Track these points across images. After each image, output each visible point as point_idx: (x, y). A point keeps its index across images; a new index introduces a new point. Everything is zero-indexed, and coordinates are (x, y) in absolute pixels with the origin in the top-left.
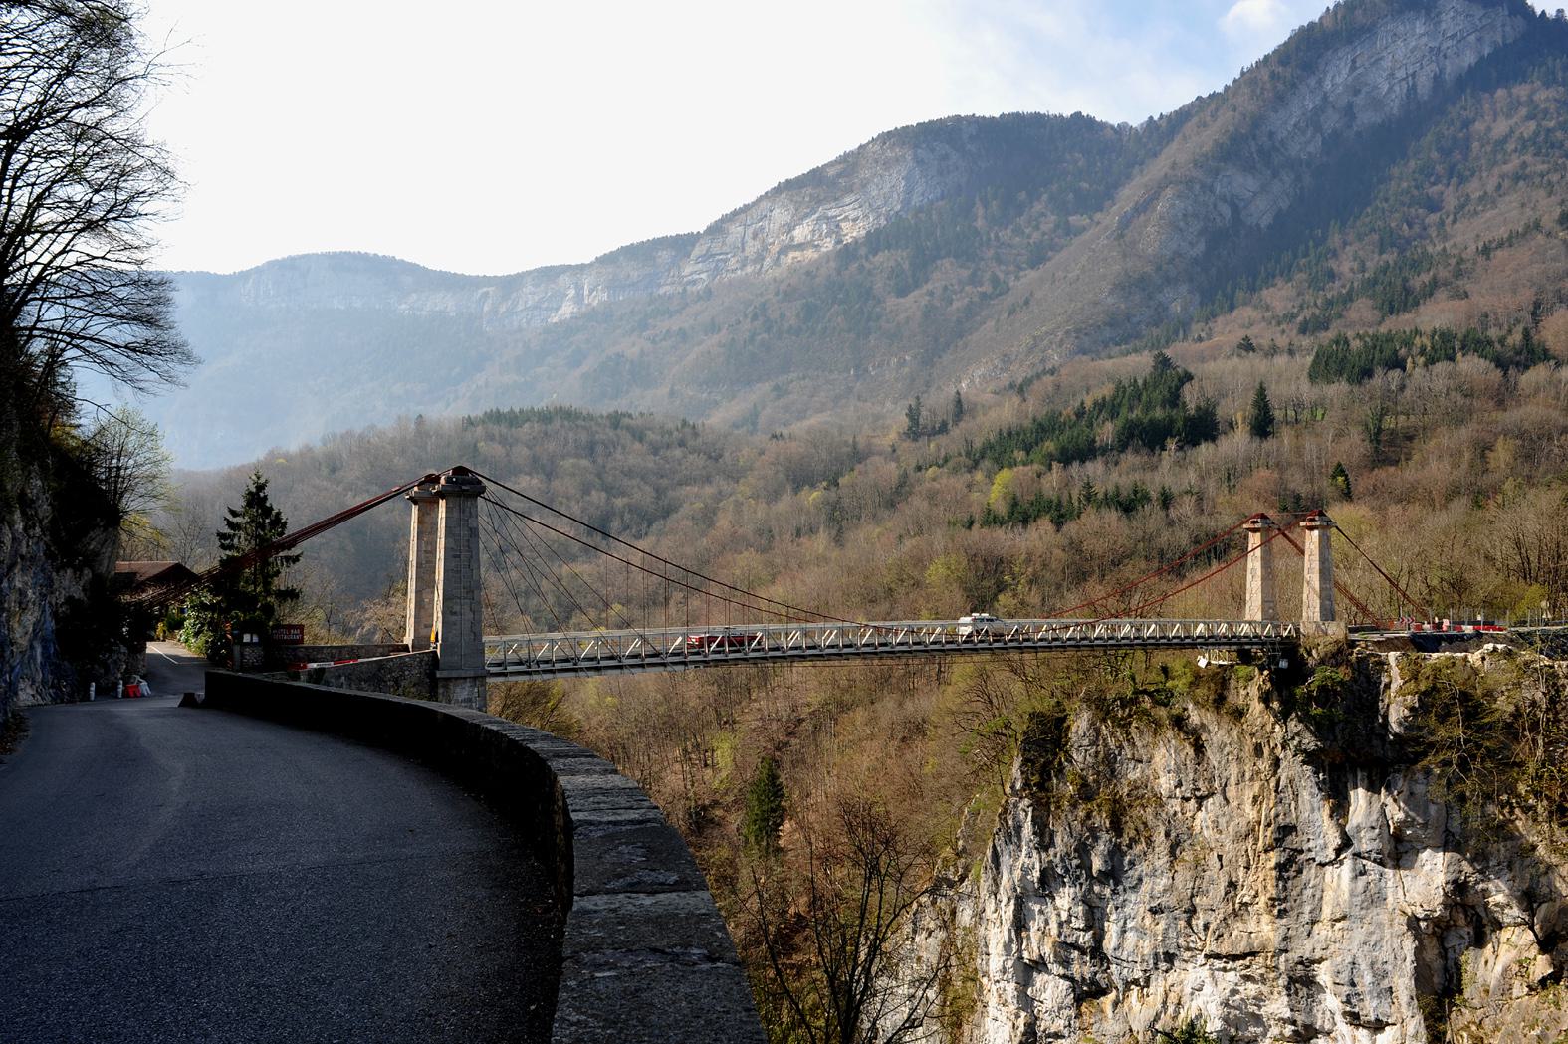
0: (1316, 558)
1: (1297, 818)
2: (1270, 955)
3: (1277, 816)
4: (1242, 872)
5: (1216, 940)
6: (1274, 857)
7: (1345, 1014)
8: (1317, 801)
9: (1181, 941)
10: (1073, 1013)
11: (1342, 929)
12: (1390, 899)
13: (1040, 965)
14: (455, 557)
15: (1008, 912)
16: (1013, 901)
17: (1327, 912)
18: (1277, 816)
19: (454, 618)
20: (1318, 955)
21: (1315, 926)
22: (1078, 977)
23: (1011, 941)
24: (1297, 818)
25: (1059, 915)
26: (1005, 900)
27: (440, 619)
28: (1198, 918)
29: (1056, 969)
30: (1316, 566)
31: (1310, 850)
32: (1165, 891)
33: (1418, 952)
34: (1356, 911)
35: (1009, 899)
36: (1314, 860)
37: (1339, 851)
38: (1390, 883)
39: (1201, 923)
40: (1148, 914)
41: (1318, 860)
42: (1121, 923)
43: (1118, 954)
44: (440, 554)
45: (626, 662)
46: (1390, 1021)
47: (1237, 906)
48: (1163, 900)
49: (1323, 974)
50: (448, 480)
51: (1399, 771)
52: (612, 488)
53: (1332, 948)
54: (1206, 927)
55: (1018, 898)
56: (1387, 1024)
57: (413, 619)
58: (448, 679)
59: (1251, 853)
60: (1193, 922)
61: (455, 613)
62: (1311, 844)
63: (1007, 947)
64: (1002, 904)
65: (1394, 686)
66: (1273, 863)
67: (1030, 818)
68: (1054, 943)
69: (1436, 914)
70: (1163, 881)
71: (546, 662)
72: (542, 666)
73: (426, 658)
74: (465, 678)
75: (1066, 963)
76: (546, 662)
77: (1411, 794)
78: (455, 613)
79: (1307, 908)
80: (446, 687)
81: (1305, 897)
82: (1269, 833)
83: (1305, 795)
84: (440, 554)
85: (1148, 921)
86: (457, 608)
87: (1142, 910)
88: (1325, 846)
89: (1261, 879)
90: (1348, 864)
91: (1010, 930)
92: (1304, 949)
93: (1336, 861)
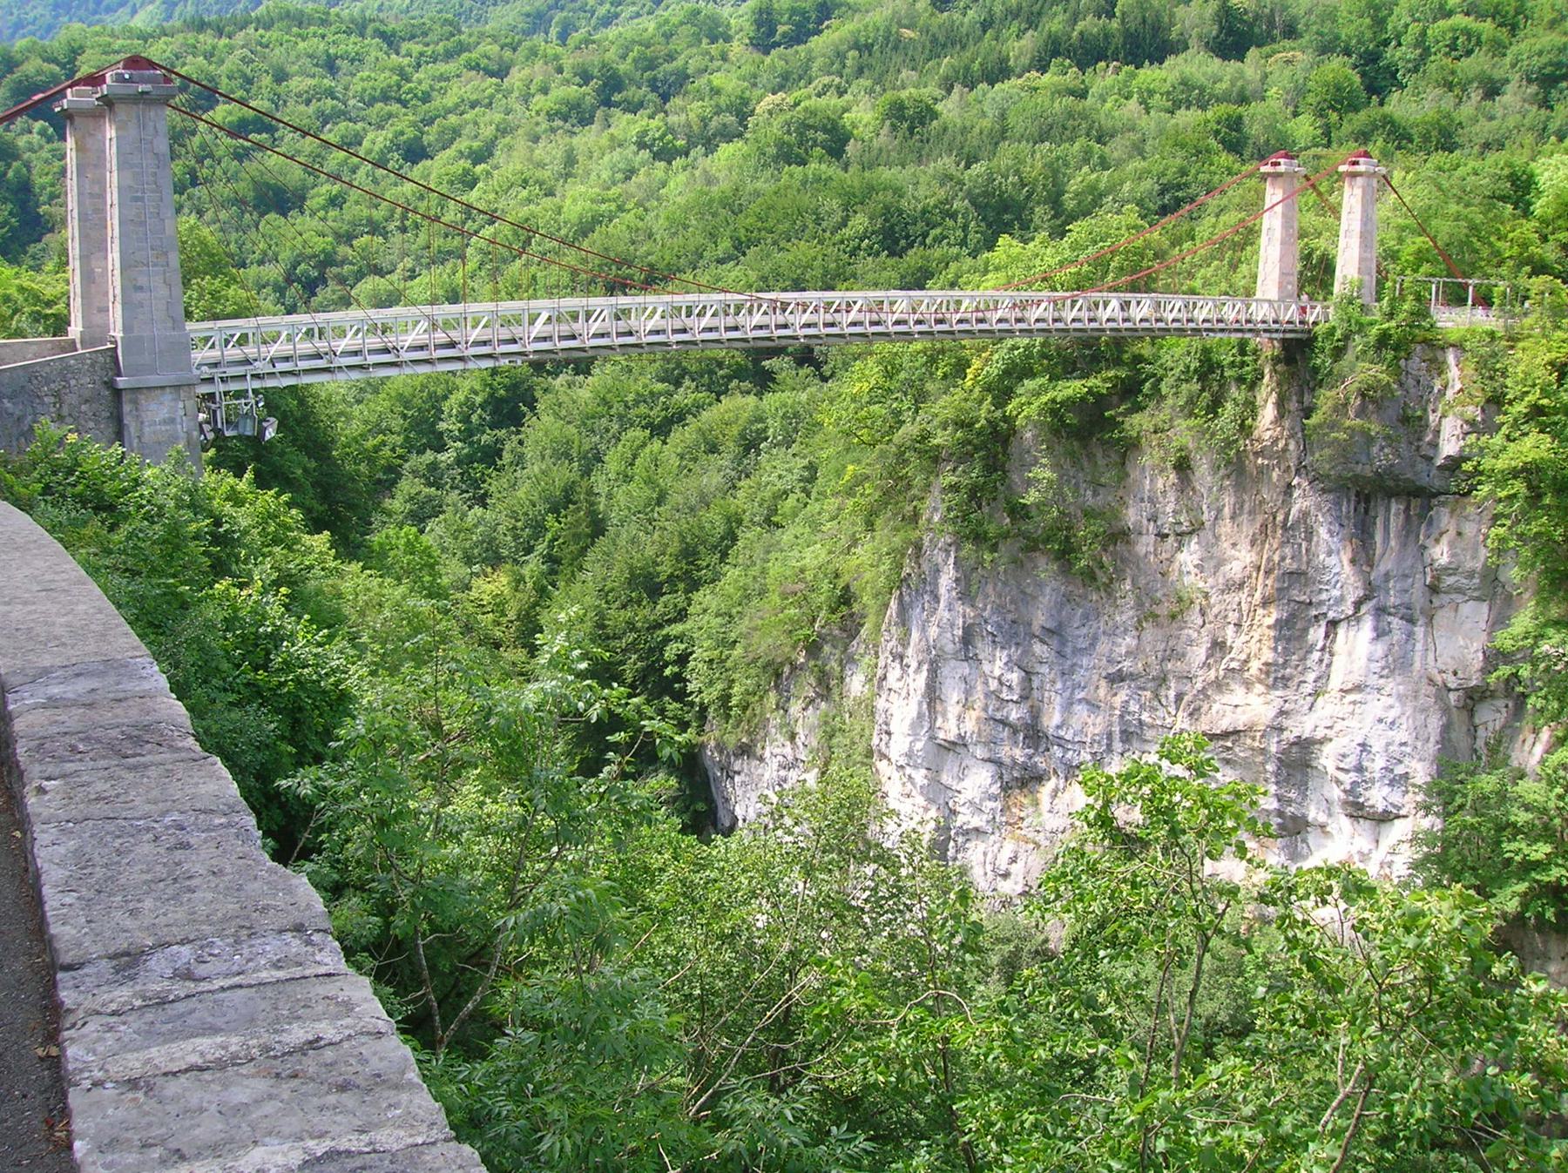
0: (1357, 215)
1: (1308, 563)
2: (1258, 734)
3: (1283, 559)
4: (1230, 630)
5: (1191, 714)
6: (1273, 615)
7: (1345, 803)
8: (1334, 543)
9: (1145, 717)
10: (998, 805)
11: (1354, 703)
12: (1417, 665)
13: (956, 746)
14: (136, 199)
15: (920, 681)
16: (925, 667)
17: (1335, 682)
18: (1283, 559)
19: (140, 296)
20: (1319, 734)
21: (1320, 699)
22: (1007, 761)
23: (920, 716)
24: (1308, 563)
25: (986, 683)
26: (914, 665)
27: (119, 298)
28: (1168, 688)
29: (980, 752)
30: (1356, 226)
31: (1321, 603)
32: (1128, 653)
33: (1446, 729)
34: (1373, 680)
35: (920, 664)
36: (1325, 614)
37: (1358, 605)
38: (1419, 646)
39: (1172, 694)
40: (1103, 683)
41: (1331, 615)
42: (1067, 694)
43: (1062, 733)
44: (113, 196)
45: (406, 356)
46: (1402, 812)
47: (1222, 673)
48: (1126, 665)
49: (1327, 758)
50: (120, 79)
51: (1443, 504)
52: (724, 555)
53: (1337, 727)
54: (1179, 697)
55: (932, 663)
56: (1398, 817)
57: (79, 300)
58: (136, 390)
59: (1245, 607)
60: (1163, 693)
61: (141, 288)
62: (1324, 596)
63: (916, 725)
64: (911, 671)
65: (1450, 394)
66: (1270, 621)
67: (951, 560)
68: (978, 719)
69: (1474, 683)
70: (1129, 641)
71: (287, 359)
72: (281, 367)
73: (101, 359)
74: (162, 388)
75: (992, 742)
76: (287, 359)
77: (1459, 534)
78: (141, 288)
79: (1311, 677)
80: (135, 402)
81: (1309, 663)
82: (1269, 582)
83: (1323, 532)
84: (113, 196)
85: (1102, 692)
86: (142, 281)
87: (1095, 677)
88: (1342, 599)
89: (1257, 638)
90: (1368, 625)
91: (920, 703)
92: (1303, 726)
93: (1355, 618)
